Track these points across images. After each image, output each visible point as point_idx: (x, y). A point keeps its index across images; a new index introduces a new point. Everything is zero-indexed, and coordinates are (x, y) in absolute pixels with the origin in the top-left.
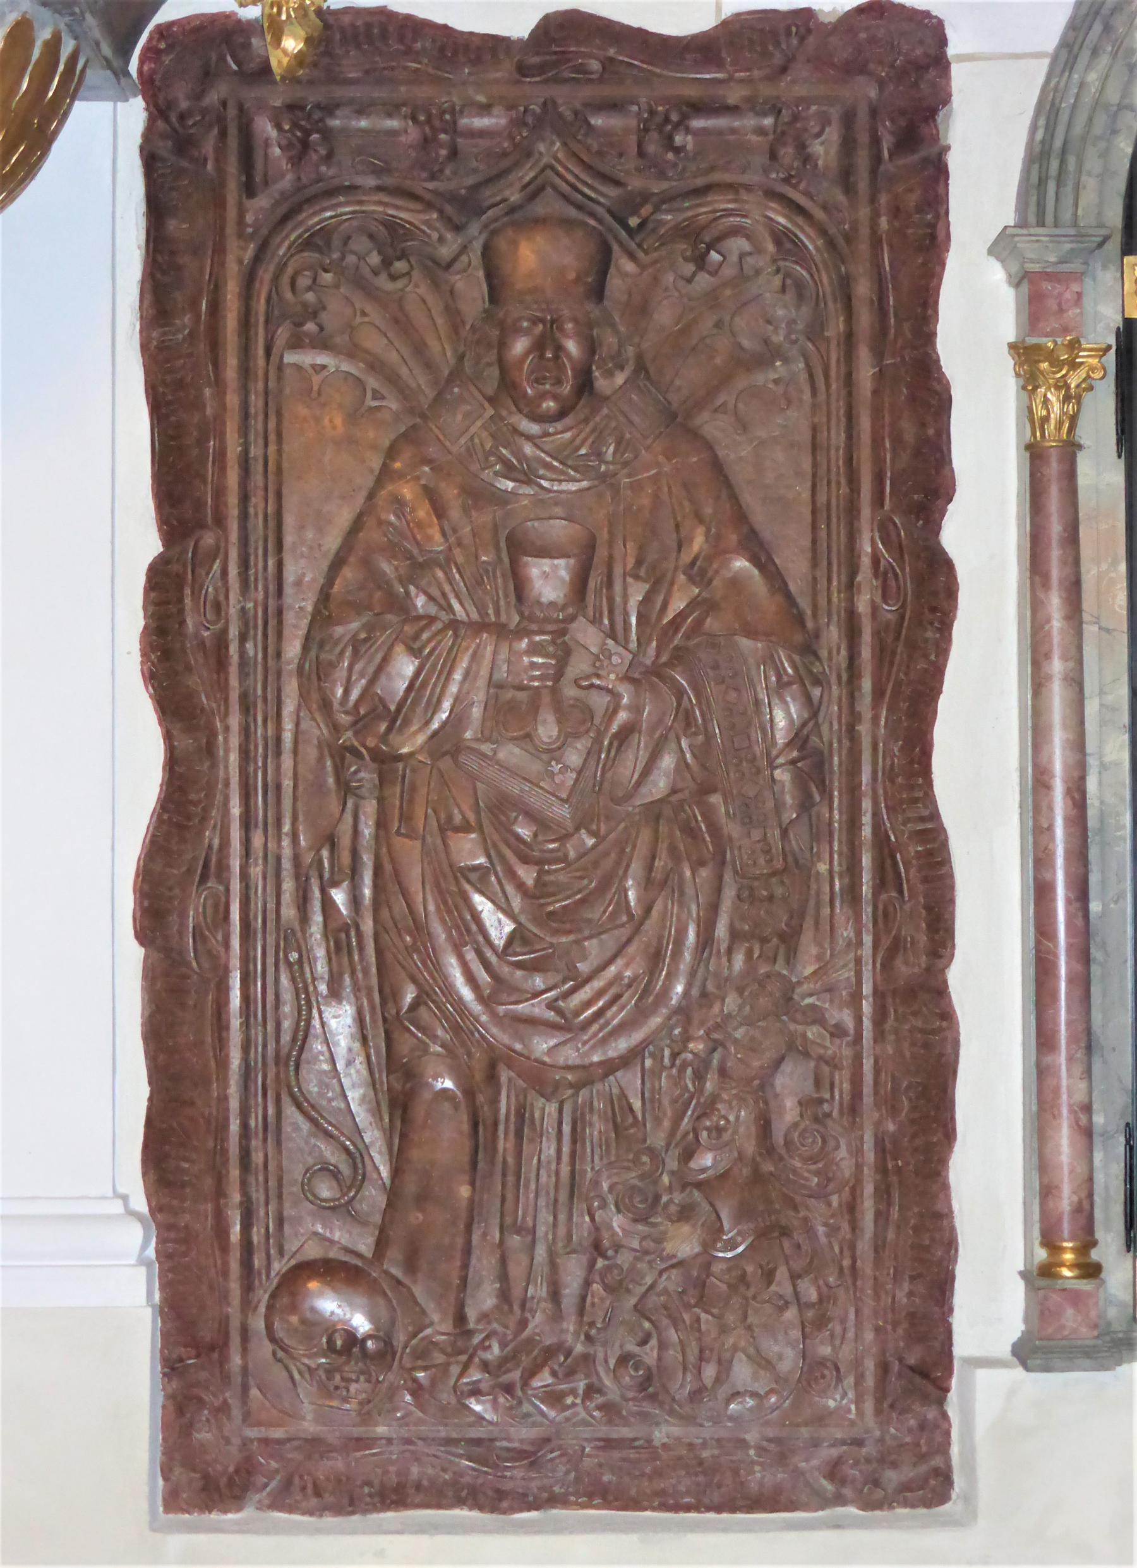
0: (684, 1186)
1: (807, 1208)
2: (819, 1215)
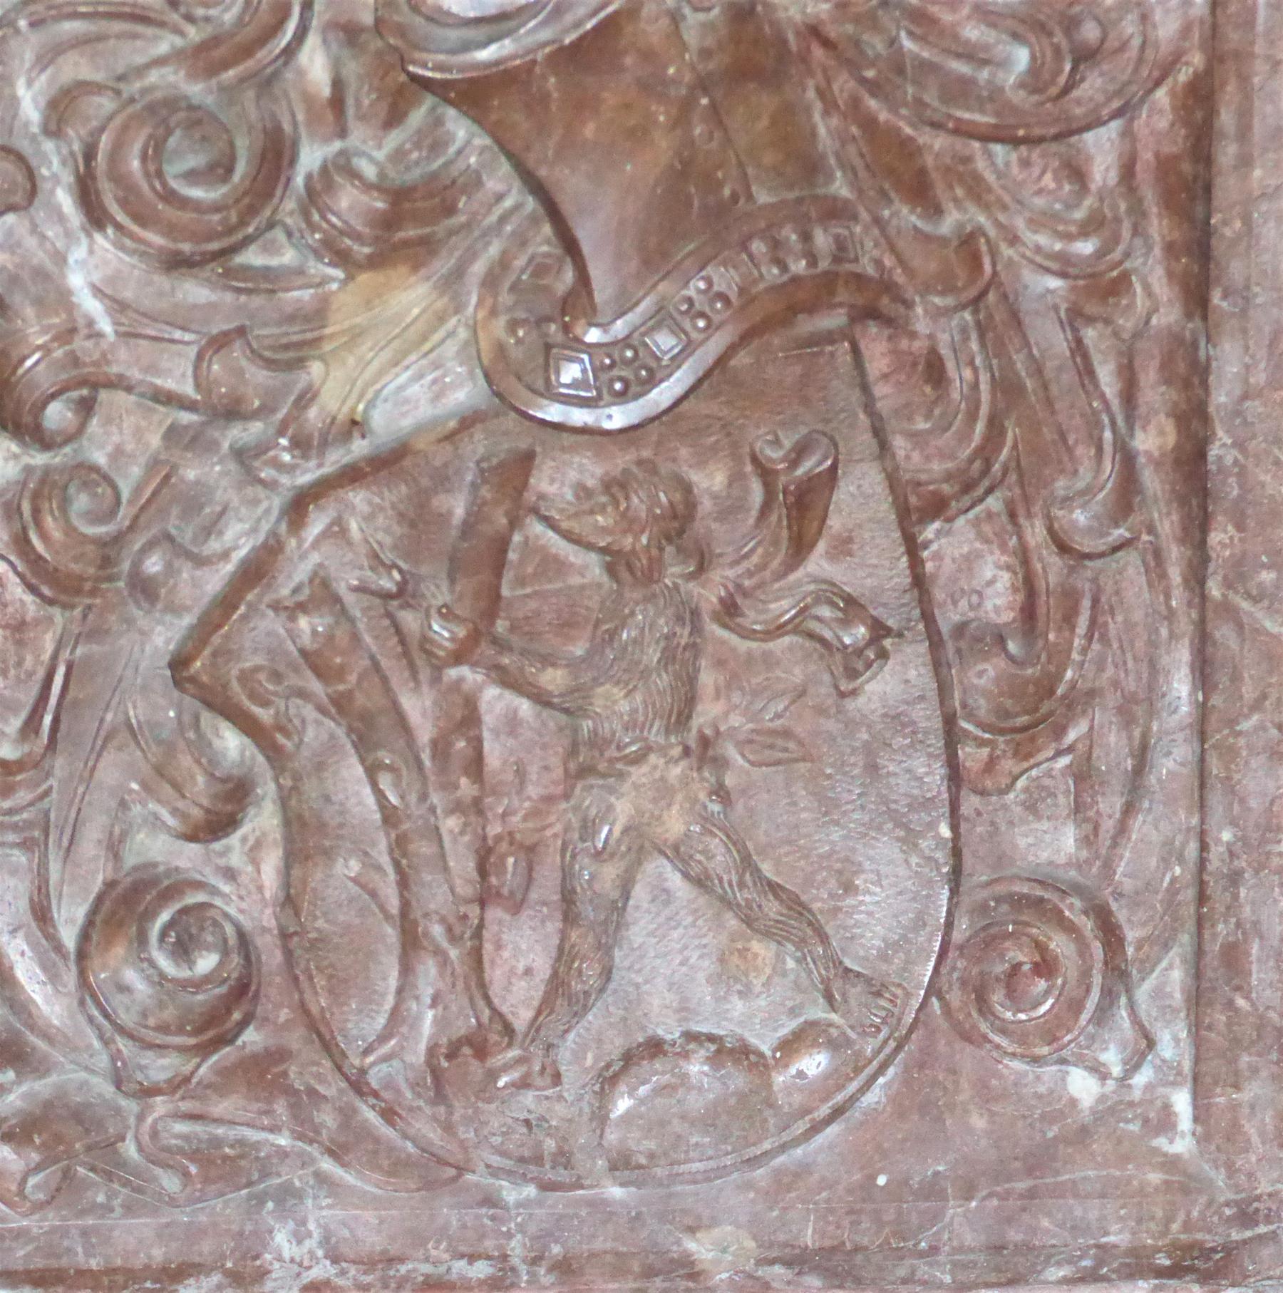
0: (401, 93)
1: (977, 190)
2: (1037, 227)
